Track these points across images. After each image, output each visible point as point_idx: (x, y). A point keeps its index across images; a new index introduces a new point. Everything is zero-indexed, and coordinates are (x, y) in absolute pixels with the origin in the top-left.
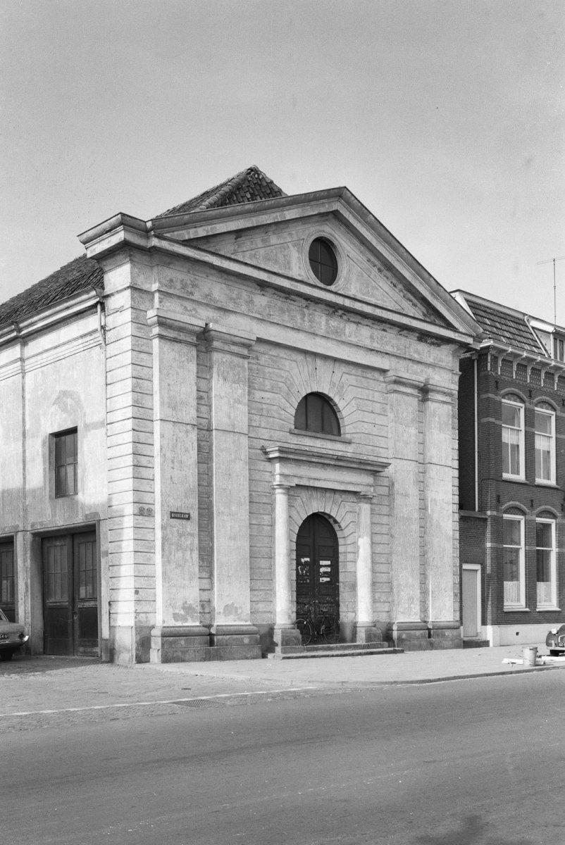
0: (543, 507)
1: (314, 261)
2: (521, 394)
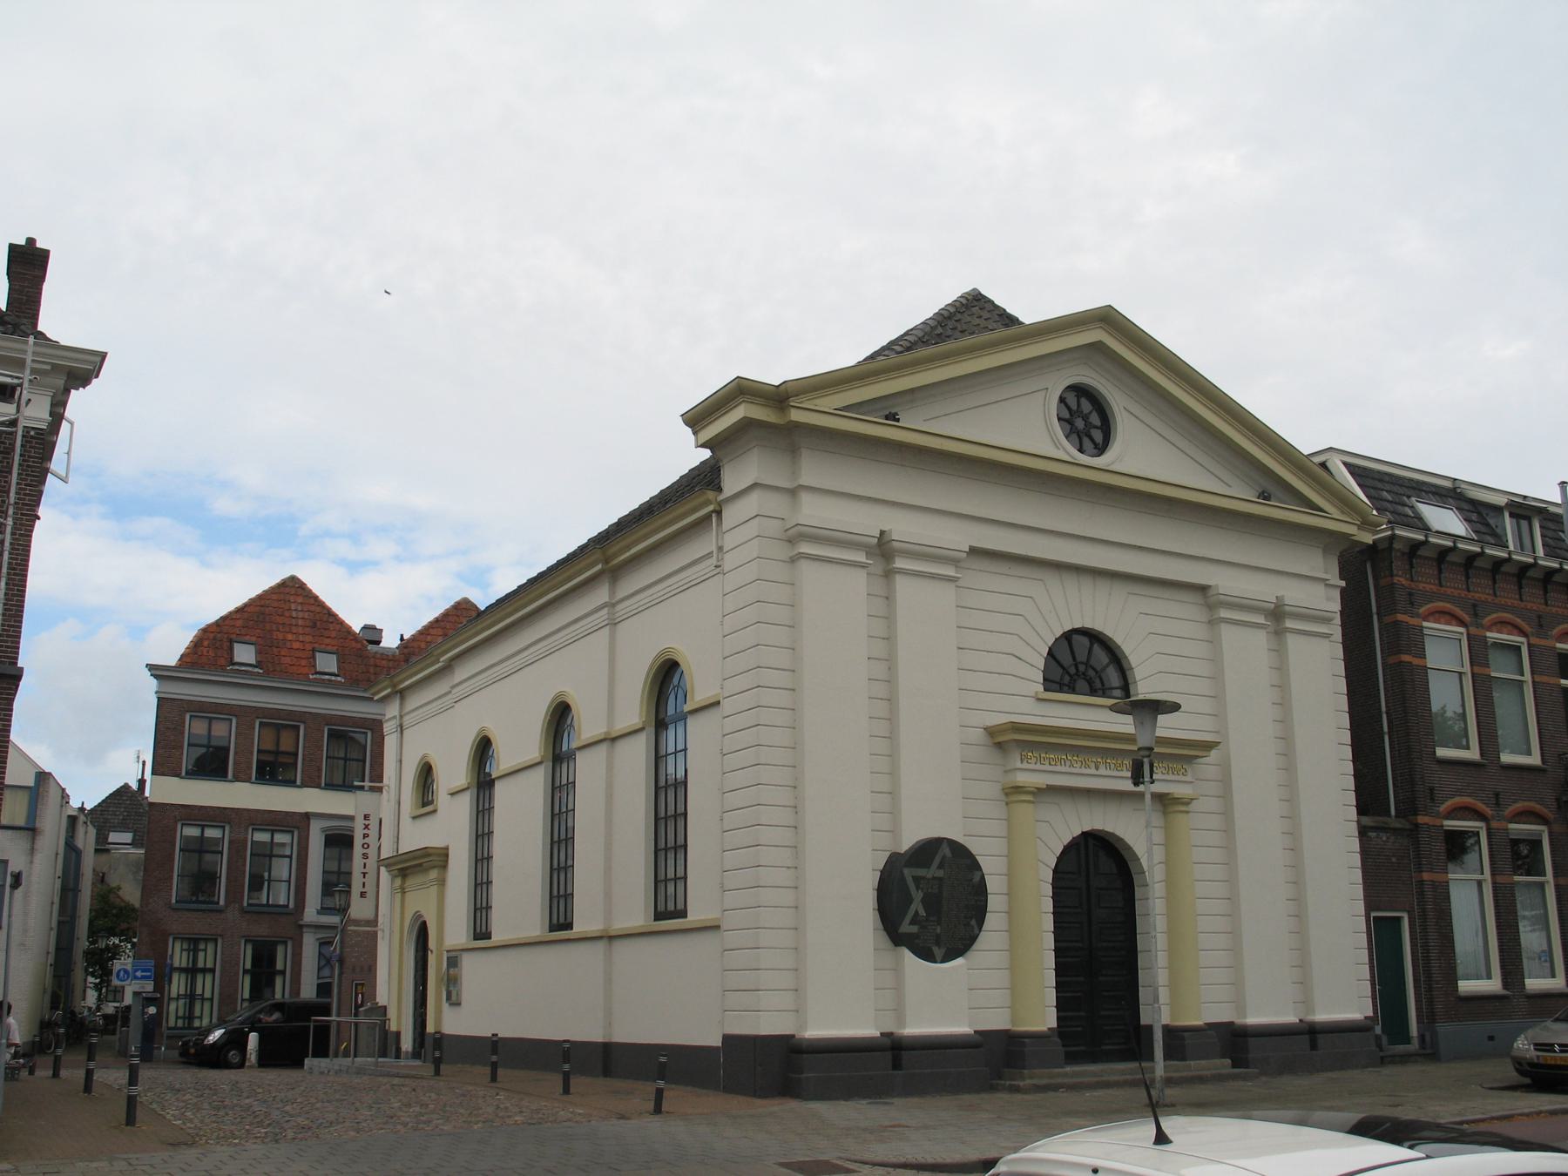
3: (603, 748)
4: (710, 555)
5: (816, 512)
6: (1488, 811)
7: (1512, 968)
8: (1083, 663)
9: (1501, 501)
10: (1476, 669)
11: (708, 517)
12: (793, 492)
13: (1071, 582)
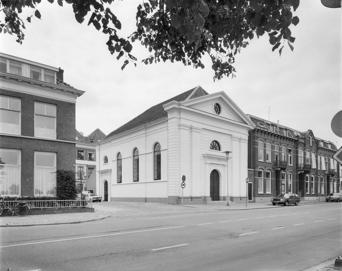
0: (268, 168)
1: (215, 108)
2: (263, 140)
3: (145, 155)
5: (183, 122)
6: (264, 169)
8: (216, 145)
9: (270, 123)
10: (280, 152)
11: (166, 121)
12: (180, 119)
13: (216, 133)
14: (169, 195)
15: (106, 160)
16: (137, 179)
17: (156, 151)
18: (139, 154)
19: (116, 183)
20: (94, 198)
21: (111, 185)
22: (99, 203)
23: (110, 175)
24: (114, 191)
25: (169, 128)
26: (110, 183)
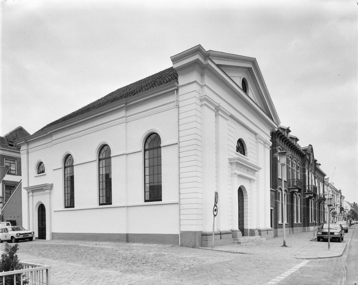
4: (174, 101)
7: (70, 205)
11: (174, 90)
14: (185, 229)
15: (40, 169)
16: (107, 198)
17: (103, 159)
18: (74, 164)
19: (62, 208)
20: (20, 234)
21: (53, 212)
22: (30, 243)
23: (50, 193)
24: (59, 222)
25: (181, 104)
26: (51, 209)
